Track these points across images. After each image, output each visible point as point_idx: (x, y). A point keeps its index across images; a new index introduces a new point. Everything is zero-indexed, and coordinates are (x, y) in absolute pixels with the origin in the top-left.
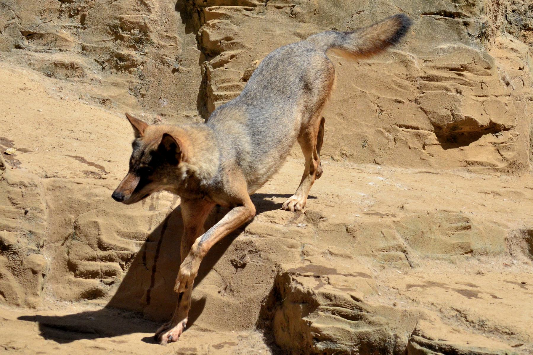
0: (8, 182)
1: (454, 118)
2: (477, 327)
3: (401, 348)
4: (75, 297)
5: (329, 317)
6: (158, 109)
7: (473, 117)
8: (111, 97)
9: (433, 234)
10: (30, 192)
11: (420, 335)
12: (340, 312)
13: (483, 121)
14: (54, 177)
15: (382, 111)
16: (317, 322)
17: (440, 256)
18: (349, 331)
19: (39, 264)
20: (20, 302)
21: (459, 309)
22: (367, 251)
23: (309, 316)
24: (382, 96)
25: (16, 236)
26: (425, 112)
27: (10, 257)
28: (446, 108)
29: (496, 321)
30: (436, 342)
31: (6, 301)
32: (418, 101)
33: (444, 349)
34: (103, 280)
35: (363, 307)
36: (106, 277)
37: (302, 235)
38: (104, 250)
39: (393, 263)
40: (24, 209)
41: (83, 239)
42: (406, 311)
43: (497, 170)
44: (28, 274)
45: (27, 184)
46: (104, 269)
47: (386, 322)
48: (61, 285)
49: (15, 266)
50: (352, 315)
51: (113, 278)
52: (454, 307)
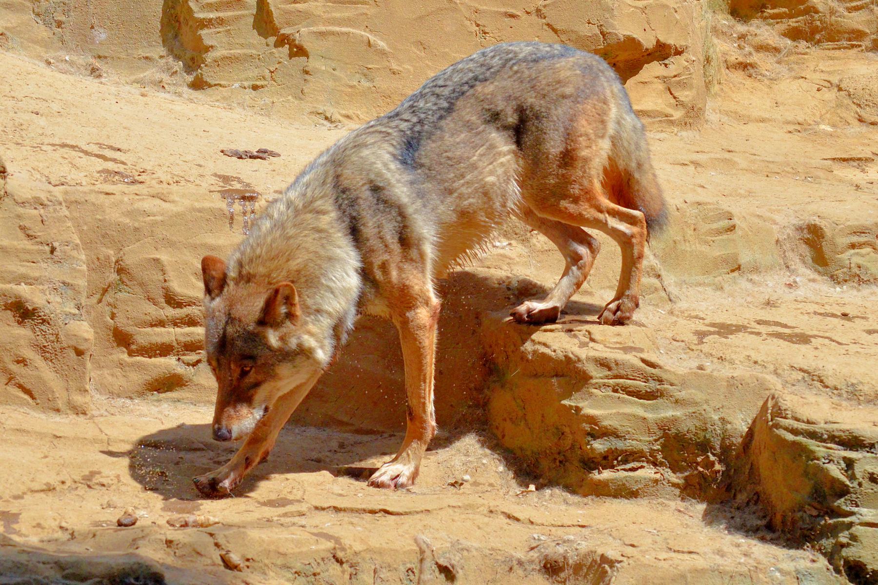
0: (14, 200)
1: (605, 40)
2: (845, 395)
3: (733, 439)
4: (136, 389)
5: (609, 396)
6: (91, 47)
7: (635, 36)
8: (7, 28)
9: (687, 244)
10: (54, 215)
11: (789, 416)
12: (627, 388)
13: (648, 42)
14: (63, 185)
15: (485, 33)
16: (591, 407)
17: (701, 278)
18: (645, 418)
19: (87, 338)
20: (60, 404)
21: (806, 368)
22: (610, 280)
23: (573, 398)
24: (482, 8)
25: (43, 292)
26: (555, 31)
27: (37, 329)
28: (589, 23)
29: (873, 383)
30: (821, 427)
31: (37, 404)
32: (543, 12)
33: (838, 437)
34: (182, 357)
35: (664, 376)
36: (186, 352)
37: (511, 261)
38: (177, 307)
39: (647, 297)
40: (48, 245)
41: (138, 289)
42: (733, 377)
43: (672, 123)
44: (69, 355)
45: (46, 202)
46: (182, 339)
47: (704, 398)
48: (106, 372)
49: (47, 344)
50: (646, 391)
51: (199, 353)
52: (795, 366)
